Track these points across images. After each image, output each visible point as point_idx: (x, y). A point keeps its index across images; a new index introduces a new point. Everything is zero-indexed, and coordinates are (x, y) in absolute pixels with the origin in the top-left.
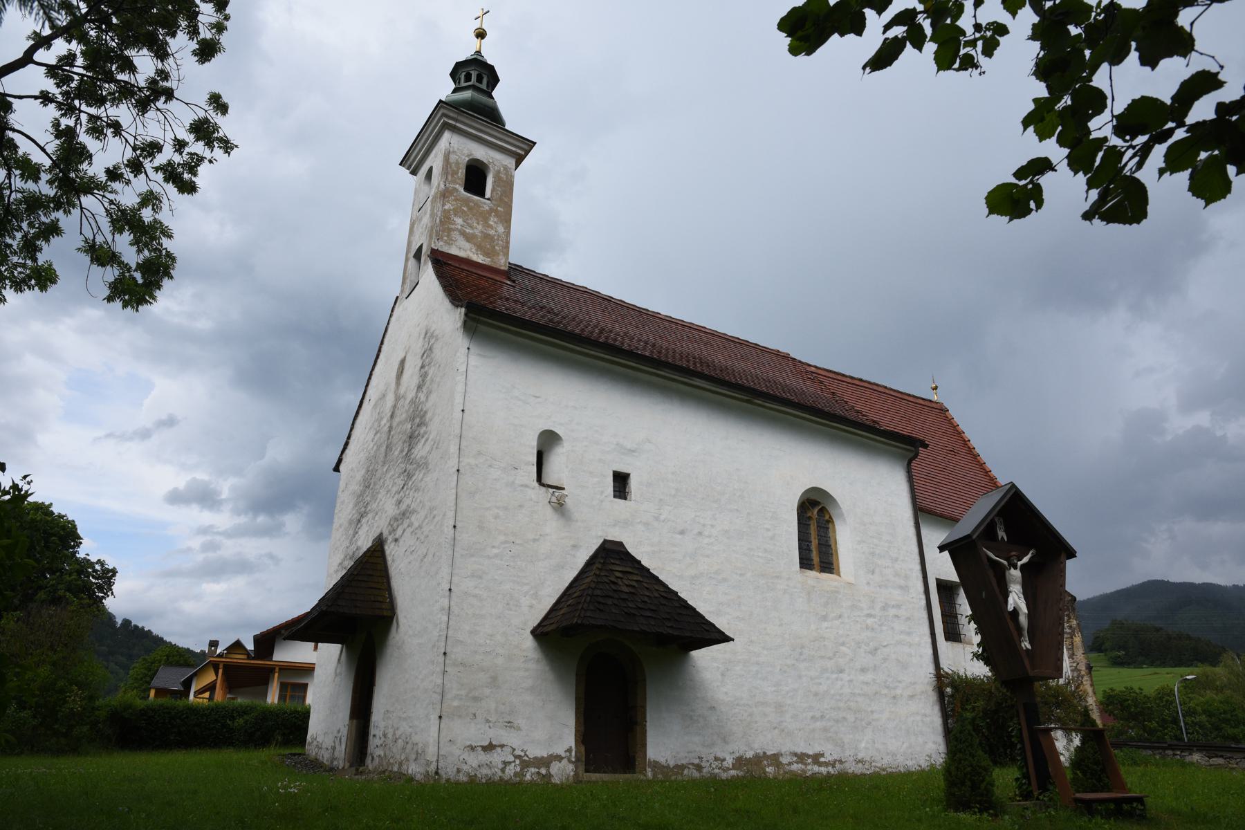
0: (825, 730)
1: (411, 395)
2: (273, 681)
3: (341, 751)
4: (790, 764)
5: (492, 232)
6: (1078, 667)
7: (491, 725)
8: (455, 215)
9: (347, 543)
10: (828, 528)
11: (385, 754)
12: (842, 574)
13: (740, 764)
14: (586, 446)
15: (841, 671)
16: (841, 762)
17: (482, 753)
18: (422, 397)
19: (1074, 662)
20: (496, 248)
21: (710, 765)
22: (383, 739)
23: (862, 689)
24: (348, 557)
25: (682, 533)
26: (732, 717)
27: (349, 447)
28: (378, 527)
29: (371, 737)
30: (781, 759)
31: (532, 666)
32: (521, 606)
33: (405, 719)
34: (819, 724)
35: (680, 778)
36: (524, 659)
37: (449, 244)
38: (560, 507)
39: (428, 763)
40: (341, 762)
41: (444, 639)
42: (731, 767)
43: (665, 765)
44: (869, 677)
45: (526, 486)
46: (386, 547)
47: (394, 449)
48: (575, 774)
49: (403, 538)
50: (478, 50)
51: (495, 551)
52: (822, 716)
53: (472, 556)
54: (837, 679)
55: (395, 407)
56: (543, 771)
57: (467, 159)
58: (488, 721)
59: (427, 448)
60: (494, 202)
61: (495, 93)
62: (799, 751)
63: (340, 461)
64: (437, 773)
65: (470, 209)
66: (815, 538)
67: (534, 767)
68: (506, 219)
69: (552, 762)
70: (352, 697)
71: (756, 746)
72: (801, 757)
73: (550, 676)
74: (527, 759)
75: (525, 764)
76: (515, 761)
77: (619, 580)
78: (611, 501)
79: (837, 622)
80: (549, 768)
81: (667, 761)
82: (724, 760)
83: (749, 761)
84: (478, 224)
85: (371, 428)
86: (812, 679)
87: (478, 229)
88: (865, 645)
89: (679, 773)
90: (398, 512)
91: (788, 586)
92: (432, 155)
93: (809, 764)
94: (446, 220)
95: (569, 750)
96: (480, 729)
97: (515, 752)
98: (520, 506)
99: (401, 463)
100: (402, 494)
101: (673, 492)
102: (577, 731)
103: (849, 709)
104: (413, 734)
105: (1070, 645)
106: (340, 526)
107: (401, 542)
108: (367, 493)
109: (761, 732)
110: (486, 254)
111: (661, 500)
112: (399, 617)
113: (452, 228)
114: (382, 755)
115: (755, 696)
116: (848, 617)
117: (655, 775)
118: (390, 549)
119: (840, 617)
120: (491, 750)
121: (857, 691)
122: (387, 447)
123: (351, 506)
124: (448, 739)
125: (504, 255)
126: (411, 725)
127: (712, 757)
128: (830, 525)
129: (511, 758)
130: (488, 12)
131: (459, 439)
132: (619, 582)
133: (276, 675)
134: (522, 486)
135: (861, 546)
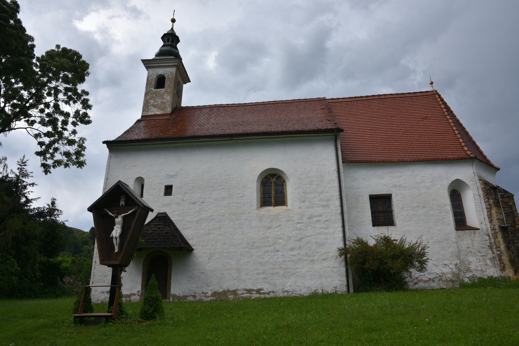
3: (345, 289)
4: (242, 294)
6: (494, 228)
13: (215, 295)
14: (153, 179)
16: (273, 292)
19: (492, 225)
25: (194, 203)
26: (212, 276)
30: (237, 292)
34: (261, 276)
42: (210, 296)
43: (179, 295)
44: (295, 252)
54: (274, 255)
62: (248, 288)
65: (156, 95)
71: (224, 287)
72: (250, 291)
78: (163, 197)
81: (179, 294)
86: (259, 256)
93: (253, 294)
95: (139, 292)
105: (490, 215)
116: (285, 226)
117: (173, 300)
130: (174, 10)
135: (297, 190)
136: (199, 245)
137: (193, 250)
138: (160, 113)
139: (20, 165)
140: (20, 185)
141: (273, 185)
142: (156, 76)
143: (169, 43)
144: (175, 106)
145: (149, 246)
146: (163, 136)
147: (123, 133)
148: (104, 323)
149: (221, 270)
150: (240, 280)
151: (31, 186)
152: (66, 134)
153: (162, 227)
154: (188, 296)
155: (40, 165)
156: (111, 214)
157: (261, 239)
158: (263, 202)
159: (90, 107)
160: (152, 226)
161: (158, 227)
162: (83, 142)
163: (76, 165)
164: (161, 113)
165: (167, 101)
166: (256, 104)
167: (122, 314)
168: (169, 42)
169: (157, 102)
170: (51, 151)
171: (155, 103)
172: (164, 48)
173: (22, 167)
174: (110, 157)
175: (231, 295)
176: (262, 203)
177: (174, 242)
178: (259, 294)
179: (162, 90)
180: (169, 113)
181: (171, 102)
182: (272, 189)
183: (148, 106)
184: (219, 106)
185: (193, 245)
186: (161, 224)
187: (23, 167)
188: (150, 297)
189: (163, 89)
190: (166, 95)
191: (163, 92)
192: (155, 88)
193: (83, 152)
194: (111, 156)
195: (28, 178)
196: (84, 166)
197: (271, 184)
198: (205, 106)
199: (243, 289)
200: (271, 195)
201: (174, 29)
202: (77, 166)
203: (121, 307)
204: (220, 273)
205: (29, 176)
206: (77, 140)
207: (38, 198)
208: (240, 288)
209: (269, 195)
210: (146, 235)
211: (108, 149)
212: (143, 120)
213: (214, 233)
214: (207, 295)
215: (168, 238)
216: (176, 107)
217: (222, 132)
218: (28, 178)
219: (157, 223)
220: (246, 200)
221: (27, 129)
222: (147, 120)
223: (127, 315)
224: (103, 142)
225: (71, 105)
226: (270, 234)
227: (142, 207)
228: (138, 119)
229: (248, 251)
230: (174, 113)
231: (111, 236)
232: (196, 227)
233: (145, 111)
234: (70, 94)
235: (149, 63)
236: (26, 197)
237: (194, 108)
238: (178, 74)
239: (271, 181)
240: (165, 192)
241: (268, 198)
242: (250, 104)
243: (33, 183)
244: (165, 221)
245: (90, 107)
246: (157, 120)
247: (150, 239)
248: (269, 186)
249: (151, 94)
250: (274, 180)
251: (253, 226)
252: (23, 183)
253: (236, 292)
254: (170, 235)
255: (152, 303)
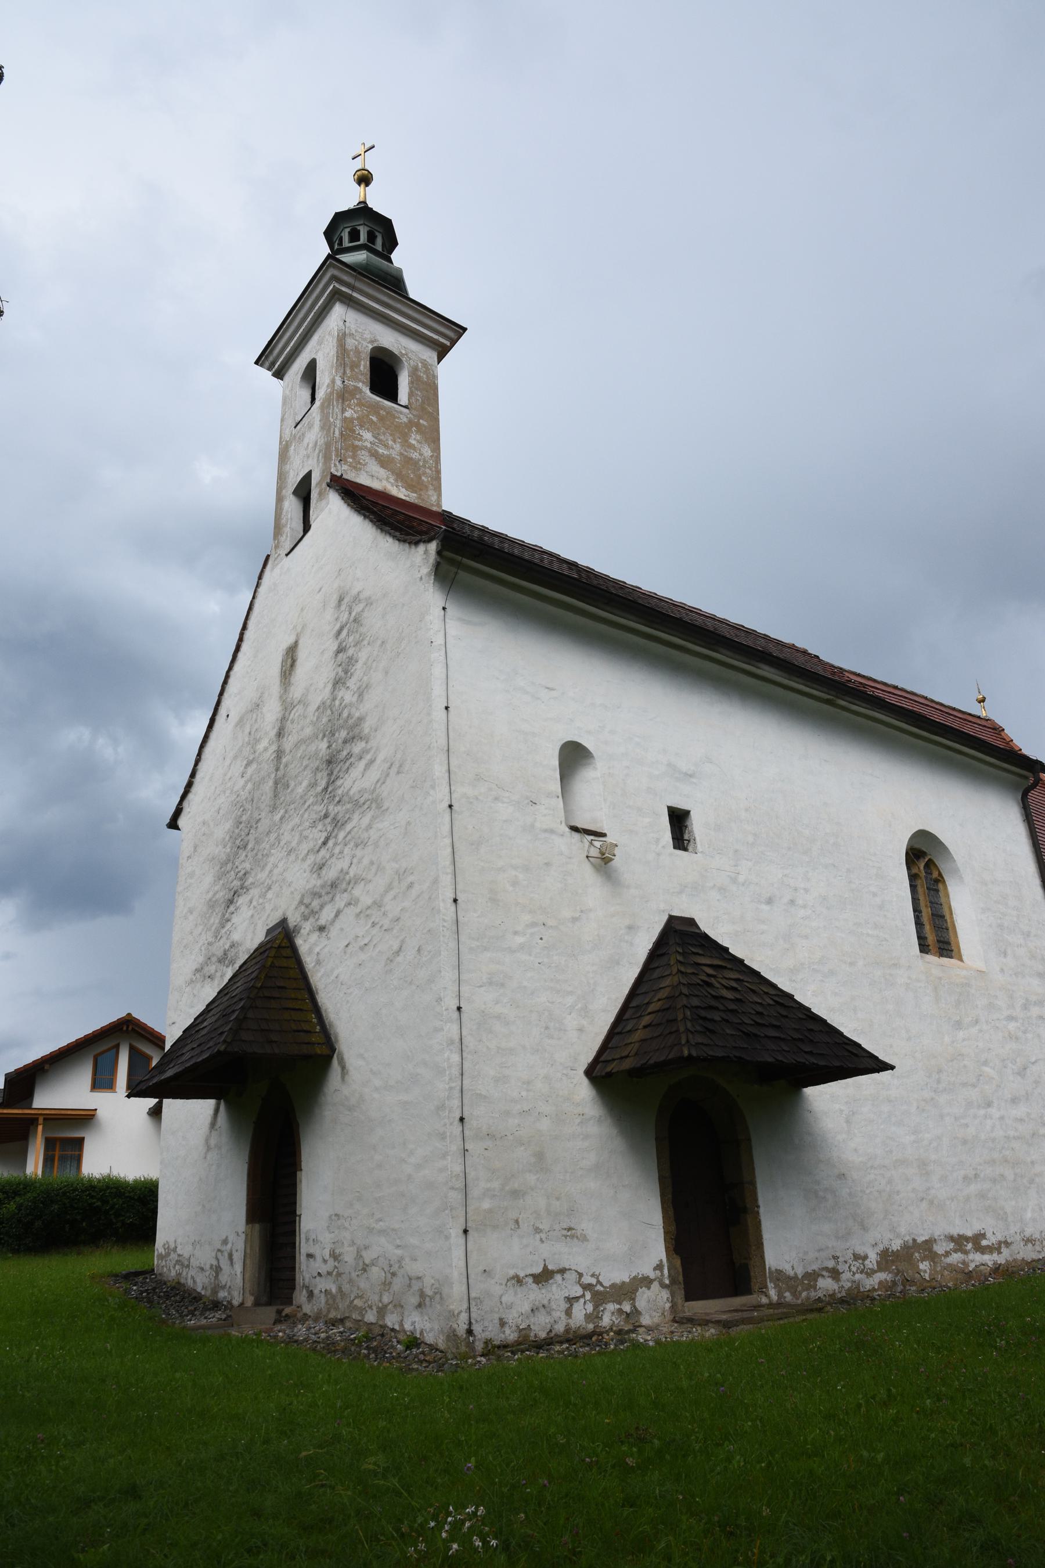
0: (982, 1196)
1: (321, 694)
2: (36, 1138)
4: (947, 1254)
5: (415, 455)
7: (543, 1236)
8: (361, 426)
9: (209, 937)
10: (937, 891)
11: (340, 1289)
12: (964, 958)
13: (887, 1261)
15: (989, 1105)
17: (534, 1286)
18: (347, 696)
20: (423, 478)
22: (331, 1263)
23: (1016, 1130)
24: (214, 959)
27: (194, 789)
28: (275, 909)
29: (302, 1259)
31: (593, 1129)
32: (565, 1030)
33: (381, 1232)
35: (813, 1295)
36: (578, 1121)
37: (355, 468)
38: (604, 861)
39: (453, 1315)
40: (235, 1294)
41: (457, 1094)
43: (792, 1273)
44: (1021, 1111)
45: (552, 831)
46: (299, 942)
47: (292, 784)
48: (672, 1307)
49: (337, 925)
50: (362, 200)
51: (520, 940)
52: (975, 1174)
53: (486, 949)
54: (985, 1117)
55: (283, 719)
56: (627, 1307)
57: (370, 347)
58: (538, 1230)
59: (374, 774)
60: (415, 413)
61: (394, 256)
62: (955, 1232)
63: (178, 812)
64: (470, 1332)
65: (382, 419)
66: (926, 906)
67: (613, 1302)
68: (433, 437)
69: (637, 1290)
70: (248, 1186)
72: (959, 1242)
73: (618, 1143)
75: (600, 1297)
76: (583, 1296)
77: (712, 979)
79: (974, 1030)
80: (634, 1299)
82: (866, 1257)
84: (394, 441)
85: (235, 757)
86: (956, 1119)
87: (395, 450)
88: (1012, 1063)
89: (811, 1286)
90: (319, 882)
91: (909, 978)
92: (315, 338)
94: (348, 431)
95: (659, 1267)
96: (527, 1246)
98: (546, 864)
99: (313, 804)
100: (323, 852)
101: (750, 839)
102: (666, 1233)
103: (1006, 1161)
104: (407, 1260)
106: (191, 912)
107: (334, 931)
108: (242, 857)
109: (906, 1208)
110: (410, 487)
111: (736, 851)
112: (346, 1057)
113: (357, 446)
114: (334, 1291)
115: (891, 1151)
118: (307, 945)
119: (977, 1022)
120: (547, 1281)
121: (1011, 1133)
122: (276, 783)
123: (209, 879)
124: (481, 1268)
125: (435, 489)
126: (398, 1242)
127: (849, 1255)
128: (940, 886)
129: (578, 1291)
130: (373, 147)
131: (446, 755)
132: (713, 980)
133: (40, 1128)
134: (546, 831)
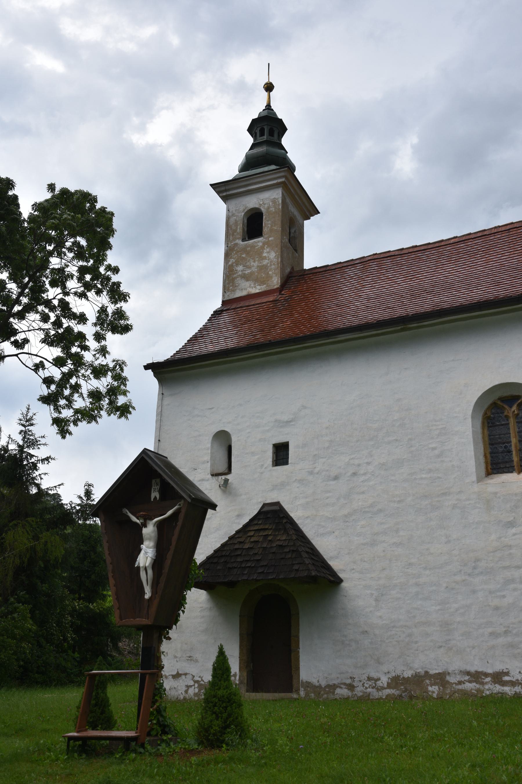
4: (460, 683)
7: (178, 659)
17: (172, 680)
21: (363, 684)
26: (387, 639)
30: (448, 678)
34: (501, 640)
42: (385, 685)
43: (317, 684)
58: (175, 657)
62: (473, 669)
65: (248, 253)
71: (416, 666)
74: (203, 683)
76: (194, 685)
78: (270, 470)
81: (318, 681)
82: (379, 679)
83: (406, 681)
86: (490, 592)
97: (194, 678)
117: (307, 695)
120: (178, 678)
127: (365, 677)
129: (192, 683)
130: (269, 64)
136: (353, 569)
137: (340, 581)
138: (258, 291)
139: (23, 425)
140: (25, 463)
141: (512, 421)
142: (243, 214)
143: (265, 138)
144: (288, 270)
145: (245, 578)
146: (262, 340)
147: (186, 342)
148: (120, 754)
149: (405, 626)
150: (450, 649)
151: (44, 463)
152: (88, 357)
153: (270, 535)
154: (337, 687)
155: (51, 422)
156: (134, 519)
157: (494, 552)
158: (492, 464)
159: (124, 297)
160: (252, 533)
161: (264, 534)
162: (122, 370)
163: (115, 415)
164: (260, 291)
165: (271, 262)
166: (464, 238)
167: (164, 732)
168: (264, 135)
169: (249, 267)
170: (67, 392)
171: (248, 271)
172: (255, 151)
173: (27, 428)
174: (162, 395)
175: (435, 684)
176: (490, 467)
177: (296, 567)
178: (499, 684)
179: (259, 242)
180: (275, 287)
181: (278, 264)
182: (512, 431)
183: (234, 279)
184: (382, 256)
185: (340, 570)
186: (270, 527)
187: (29, 427)
188: (215, 696)
189: (261, 239)
190: (268, 250)
191: (260, 244)
192: (244, 240)
193: (122, 387)
194: (163, 394)
195: (39, 448)
196: (130, 413)
197: (508, 420)
198: (352, 260)
199: (461, 671)
200: (511, 446)
201: (271, 105)
202: (117, 415)
203: (162, 716)
204: (404, 632)
205: (40, 444)
206: (111, 365)
207: (59, 485)
208: (454, 669)
209: (505, 447)
210: (239, 552)
211: (156, 379)
212: (226, 310)
213: (384, 542)
214: (379, 683)
215: (282, 558)
216: (290, 273)
217: (386, 315)
218: (39, 448)
219: (261, 527)
220: (451, 461)
221: (19, 356)
222: (232, 309)
223: (176, 735)
224: (144, 366)
225: (89, 299)
226: (514, 537)
227: (188, 502)
228: (215, 309)
229: (464, 581)
230: (286, 286)
231: (136, 566)
232: (343, 529)
233: (228, 290)
234: (88, 277)
235: (227, 187)
236: (38, 486)
237: (328, 268)
238: (288, 200)
239: (506, 414)
240: (275, 459)
241: (502, 453)
242: (452, 241)
243: (48, 457)
244: (276, 521)
245: (124, 297)
246: (253, 305)
247: (248, 561)
248: (502, 425)
249: (236, 254)
250: (514, 411)
251: (471, 522)
252: (31, 459)
253: (445, 677)
254: (288, 550)
255: (219, 709)
